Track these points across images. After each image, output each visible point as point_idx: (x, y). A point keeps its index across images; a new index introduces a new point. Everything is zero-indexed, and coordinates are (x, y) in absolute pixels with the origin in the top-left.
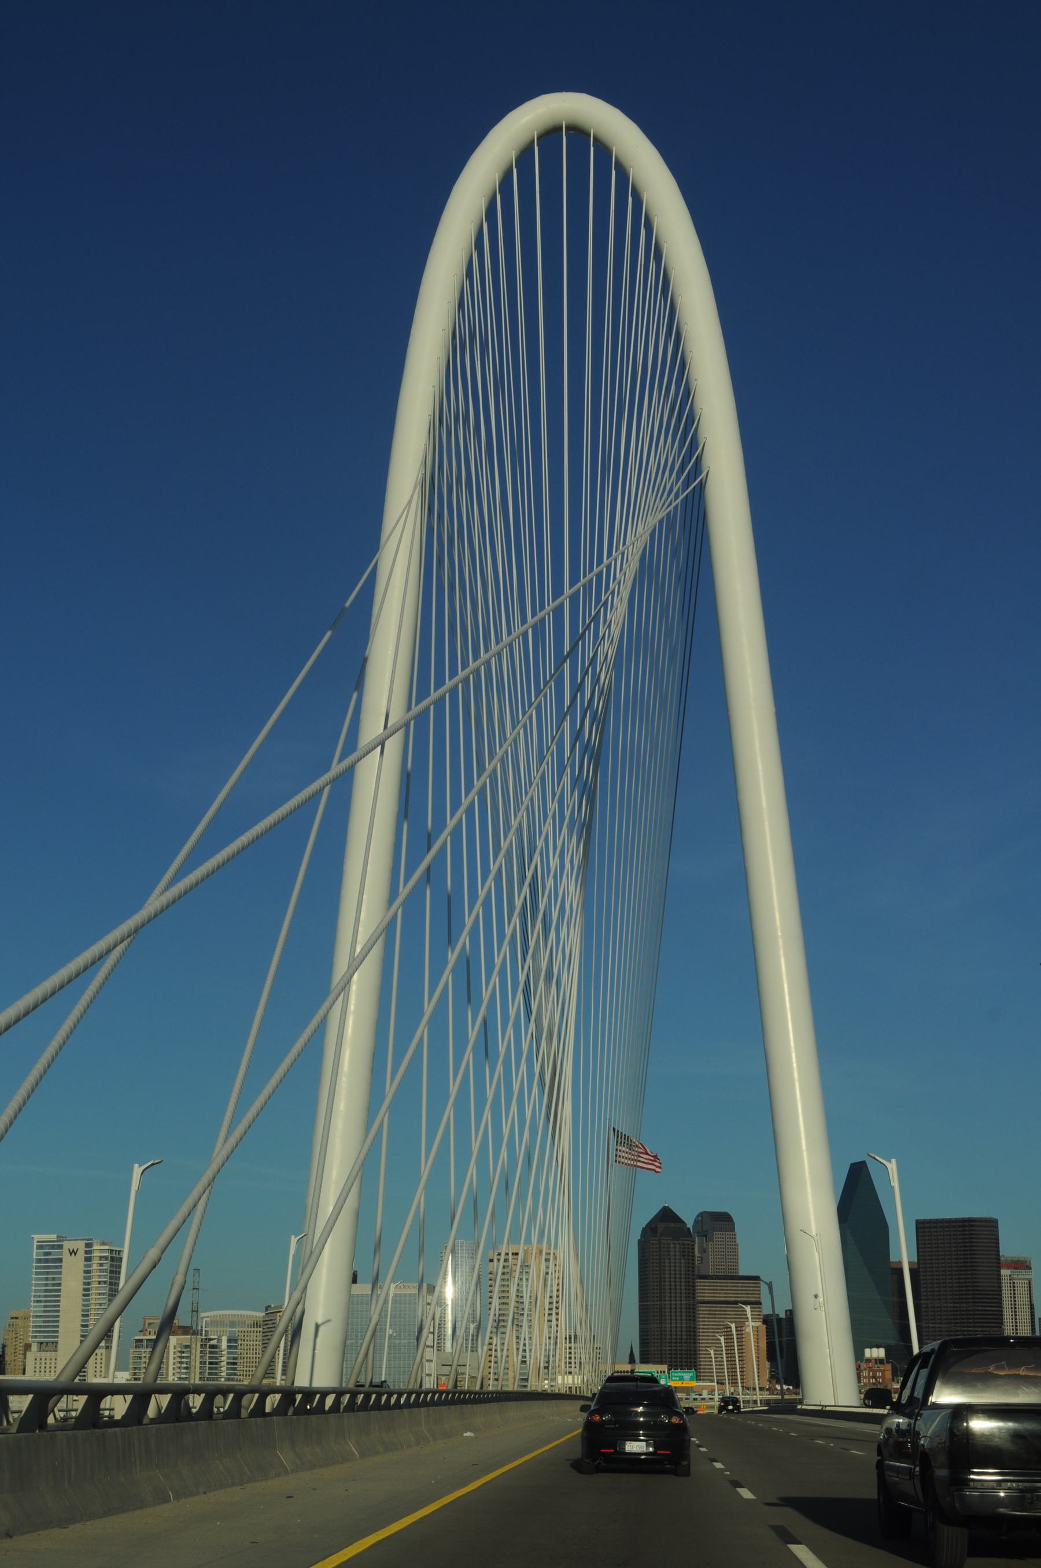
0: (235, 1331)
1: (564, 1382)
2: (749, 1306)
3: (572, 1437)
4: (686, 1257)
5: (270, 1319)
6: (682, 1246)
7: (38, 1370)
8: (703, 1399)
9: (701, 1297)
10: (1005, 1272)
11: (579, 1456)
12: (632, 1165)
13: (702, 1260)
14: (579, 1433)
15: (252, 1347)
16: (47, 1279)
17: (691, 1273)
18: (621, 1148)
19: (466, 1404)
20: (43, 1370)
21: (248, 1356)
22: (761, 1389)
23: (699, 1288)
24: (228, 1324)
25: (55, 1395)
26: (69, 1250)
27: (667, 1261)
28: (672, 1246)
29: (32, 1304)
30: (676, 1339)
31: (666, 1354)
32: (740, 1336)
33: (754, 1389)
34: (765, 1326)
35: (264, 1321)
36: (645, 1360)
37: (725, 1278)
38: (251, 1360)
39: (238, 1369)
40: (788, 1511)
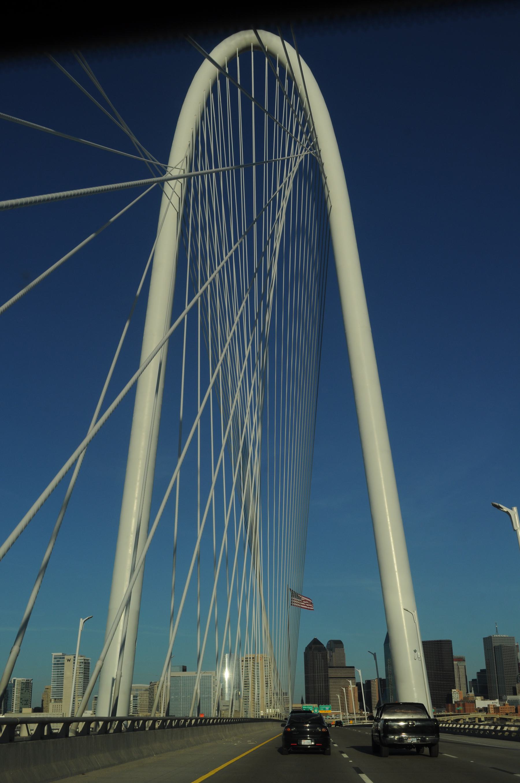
0: (138, 693)
1: (270, 711)
2: (351, 681)
3: (269, 741)
4: (324, 659)
5: (152, 687)
6: (322, 654)
7: (54, 710)
8: (333, 718)
9: (330, 675)
10: (455, 663)
11: (281, 746)
12: (298, 606)
13: (330, 660)
14: (280, 736)
15: (145, 700)
16: (58, 672)
17: (326, 665)
18: (294, 598)
19: (232, 724)
20: (56, 710)
21: (144, 703)
22: (356, 714)
23: (329, 672)
24: (135, 690)
25: (93, 722)
26: (67, 659)
27: (316, 661)
28: (318, 654)
29: (52, 682)
30: (321, 693)
31: (316, 700)
32: (347, 693)
33: (353, 713)
34: (357, 687)
35: (149, 688)
36: (308, 702)
37: (340, 667)
38: (145, 705)
39: (138, 709)
40: (352, 749)
